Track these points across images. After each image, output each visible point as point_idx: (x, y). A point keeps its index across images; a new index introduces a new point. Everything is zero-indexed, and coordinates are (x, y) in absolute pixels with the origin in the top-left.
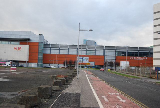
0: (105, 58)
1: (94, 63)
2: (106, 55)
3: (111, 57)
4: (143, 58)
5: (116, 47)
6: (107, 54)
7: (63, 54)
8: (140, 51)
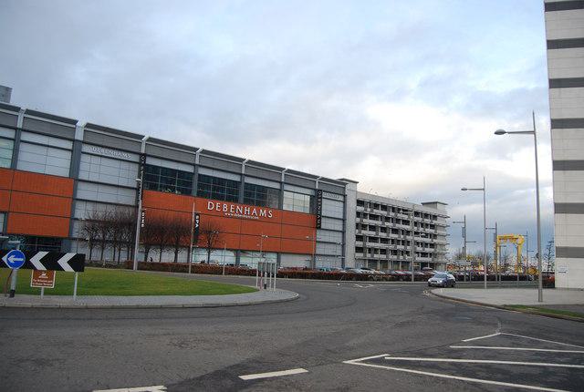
0: (79, 196)
2: (82, 176)
3: (114, 190)
4: (258, 212)
5: (81, 123)
6: (92, 168)
8: (202, 172)
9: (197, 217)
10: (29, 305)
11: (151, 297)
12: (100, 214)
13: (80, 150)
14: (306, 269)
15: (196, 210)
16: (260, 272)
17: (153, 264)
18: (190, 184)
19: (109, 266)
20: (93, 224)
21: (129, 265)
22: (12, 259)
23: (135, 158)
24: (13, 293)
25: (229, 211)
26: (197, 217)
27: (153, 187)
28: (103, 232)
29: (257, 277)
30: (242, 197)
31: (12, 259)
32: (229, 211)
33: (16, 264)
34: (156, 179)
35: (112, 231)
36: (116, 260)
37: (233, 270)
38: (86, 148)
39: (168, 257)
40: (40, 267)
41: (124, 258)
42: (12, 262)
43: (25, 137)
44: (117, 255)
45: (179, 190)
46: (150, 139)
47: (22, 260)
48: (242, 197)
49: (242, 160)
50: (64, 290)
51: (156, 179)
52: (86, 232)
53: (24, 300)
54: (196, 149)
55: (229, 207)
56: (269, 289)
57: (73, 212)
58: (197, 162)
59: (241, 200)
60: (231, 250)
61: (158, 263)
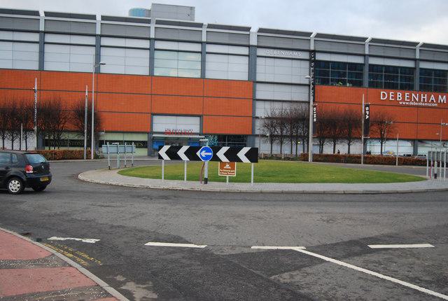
0: (258, 97)
1: (197, 120)
4: (437, 100)
5: (254, 30)
6: (265, 70)
7: (10, 67)
8: (373, 61)
9: (367, 108)
10: (218, 189)
11: (406, 183)
12: (277, 112)
13: (256, 53)
14: (409, 155)
15: (363, 101)
16: (430, 162)
17: (327, 156)
18: (361, 75)
19: (287, 158)
20: (272, 121)
21: (304, 158)
22: (204, 154)
23: (306, 55)
24: (206, 181)
25: (403, 100)
26: (367, 108)
27: (325, 82)
28: (281, 129)
29: (428, 167)
30: (417, 83)
31: (204, 154)
32: (403, 100)
33: (207, 158)
34: (327, 74)
35: (288, 127)
36: (294, 153)
37: (406, 161)
38: (260, 52)
39: (342, 148)
40: (224, 159)
41: (300, 152)
42: (204, 156)
43: (105, 41)
44: (294, 149)
45: (350, 82)
46: (318, 35)
47: (210, 154)
48: (417, 83)
49: (415, 44)
50: (242, 178)
51: (327, 74)
52: (266, 129)
53: (214, 186)
54: (364, 39)
55: (403, 96)
56: (440, 178)
57: (254, 112)
58: (367, 52)
59: (366, 83)
60: (408, 140)
61: (331, 155)
